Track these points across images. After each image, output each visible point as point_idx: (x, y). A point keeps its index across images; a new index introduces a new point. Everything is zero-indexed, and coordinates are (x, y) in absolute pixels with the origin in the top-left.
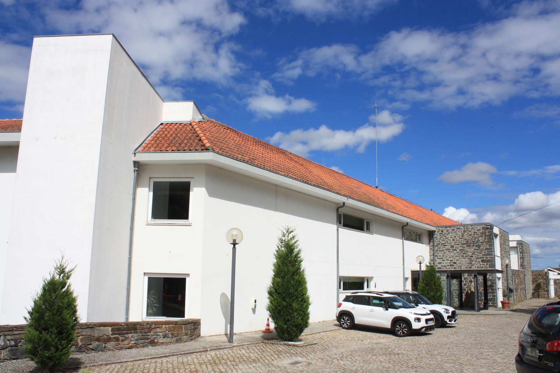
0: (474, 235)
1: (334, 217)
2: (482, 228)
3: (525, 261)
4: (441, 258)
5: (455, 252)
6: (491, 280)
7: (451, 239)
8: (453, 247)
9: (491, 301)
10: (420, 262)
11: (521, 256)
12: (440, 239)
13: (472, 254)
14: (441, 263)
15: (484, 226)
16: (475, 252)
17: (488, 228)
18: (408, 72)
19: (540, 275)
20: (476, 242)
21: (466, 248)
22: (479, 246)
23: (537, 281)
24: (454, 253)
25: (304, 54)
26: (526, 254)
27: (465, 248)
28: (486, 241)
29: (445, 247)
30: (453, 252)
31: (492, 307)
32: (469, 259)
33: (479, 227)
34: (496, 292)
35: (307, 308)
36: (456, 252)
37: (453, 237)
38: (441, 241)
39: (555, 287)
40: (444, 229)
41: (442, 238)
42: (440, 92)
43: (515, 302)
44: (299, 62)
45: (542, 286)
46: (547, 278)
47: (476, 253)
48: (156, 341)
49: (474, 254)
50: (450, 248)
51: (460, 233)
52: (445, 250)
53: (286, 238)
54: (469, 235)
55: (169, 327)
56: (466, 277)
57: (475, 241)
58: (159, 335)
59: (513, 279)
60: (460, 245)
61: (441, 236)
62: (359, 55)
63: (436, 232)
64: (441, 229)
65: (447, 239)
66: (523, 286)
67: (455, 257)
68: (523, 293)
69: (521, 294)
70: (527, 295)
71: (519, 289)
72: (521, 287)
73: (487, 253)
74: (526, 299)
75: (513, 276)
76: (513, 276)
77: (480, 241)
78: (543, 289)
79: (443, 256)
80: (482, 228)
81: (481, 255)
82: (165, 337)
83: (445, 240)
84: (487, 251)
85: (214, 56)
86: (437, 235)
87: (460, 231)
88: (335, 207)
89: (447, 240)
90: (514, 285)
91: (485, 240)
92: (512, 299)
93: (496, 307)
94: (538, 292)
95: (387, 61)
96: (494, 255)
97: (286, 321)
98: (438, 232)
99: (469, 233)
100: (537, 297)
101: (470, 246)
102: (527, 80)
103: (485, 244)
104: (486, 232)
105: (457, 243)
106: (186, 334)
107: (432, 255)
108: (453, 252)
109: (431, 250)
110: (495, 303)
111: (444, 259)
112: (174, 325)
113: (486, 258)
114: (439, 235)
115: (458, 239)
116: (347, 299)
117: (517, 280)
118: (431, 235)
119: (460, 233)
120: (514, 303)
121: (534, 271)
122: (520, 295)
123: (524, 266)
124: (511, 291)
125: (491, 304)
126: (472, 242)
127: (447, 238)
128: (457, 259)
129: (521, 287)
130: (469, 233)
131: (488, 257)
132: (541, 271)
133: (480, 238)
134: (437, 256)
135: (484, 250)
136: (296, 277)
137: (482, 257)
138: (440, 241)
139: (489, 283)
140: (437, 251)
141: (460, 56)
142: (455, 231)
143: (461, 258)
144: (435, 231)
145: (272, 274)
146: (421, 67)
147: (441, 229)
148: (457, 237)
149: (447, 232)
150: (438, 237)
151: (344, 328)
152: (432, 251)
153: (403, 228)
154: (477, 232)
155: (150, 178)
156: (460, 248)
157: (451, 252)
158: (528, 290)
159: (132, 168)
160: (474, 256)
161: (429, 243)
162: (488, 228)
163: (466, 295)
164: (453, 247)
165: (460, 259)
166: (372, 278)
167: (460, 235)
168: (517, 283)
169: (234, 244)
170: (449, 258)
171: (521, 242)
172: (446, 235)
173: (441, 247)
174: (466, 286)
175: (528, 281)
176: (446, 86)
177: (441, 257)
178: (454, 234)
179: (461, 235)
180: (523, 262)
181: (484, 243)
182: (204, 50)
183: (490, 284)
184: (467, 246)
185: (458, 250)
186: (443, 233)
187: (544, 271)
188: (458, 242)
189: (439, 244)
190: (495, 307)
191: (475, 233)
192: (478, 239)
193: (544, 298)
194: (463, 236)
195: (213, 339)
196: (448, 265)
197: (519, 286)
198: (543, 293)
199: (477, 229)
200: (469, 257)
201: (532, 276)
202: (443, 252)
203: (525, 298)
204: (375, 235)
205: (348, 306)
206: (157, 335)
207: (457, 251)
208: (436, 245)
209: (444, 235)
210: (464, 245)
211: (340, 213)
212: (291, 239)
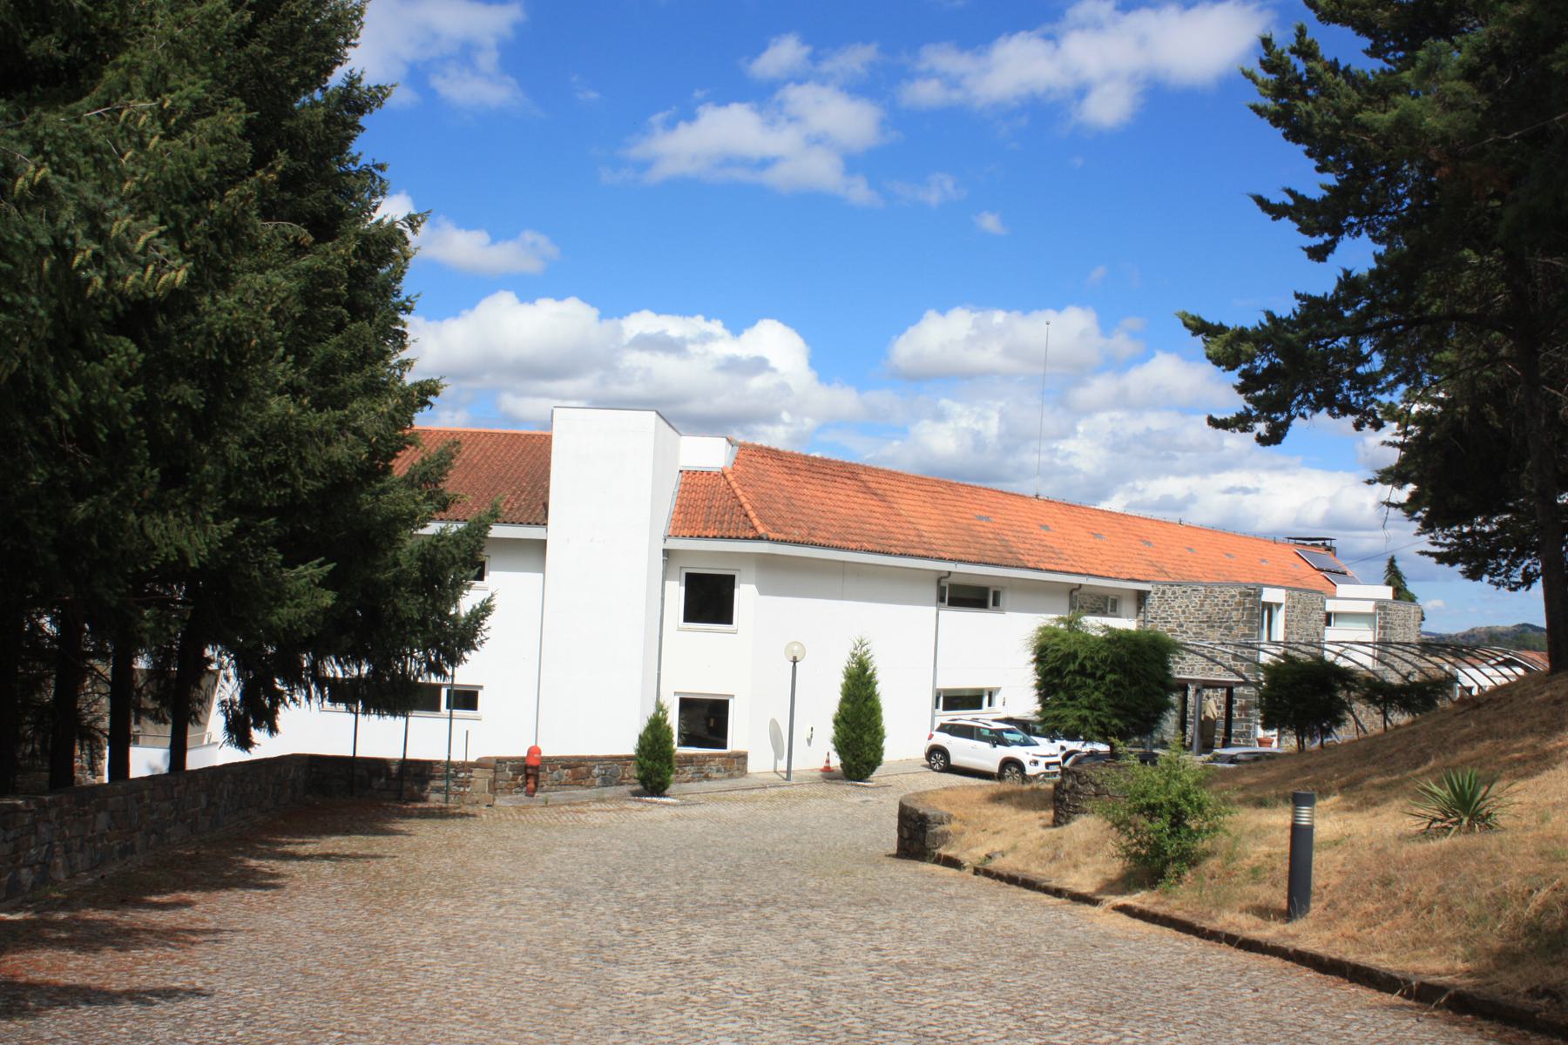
1: (933, 593)
8: (1182, 626)
15: (1243, 589)
17: (1249, 595)
22: (1230, 629)
35: (881, 741)
53: (858, 653)
64: (1162, 588)
82: (718, 771)
86: (1153, 600)
88: (935, 577)
97: (855, 757)
116: (943, 728)
133: (1234, 613)
136: (870, 704)
145: (839, 697)
147: (1162, 588)
151: (935, 770)
153: (1071, 592)
162: (1249, 595)
164: (1182, 626)
166: (999, 689)
169: (795, 661)
194: (1202, 605)
195: (760, 776)
204: (1008, 613)
205: (943, 739)
211: (942, 584)
212: (865, 654)
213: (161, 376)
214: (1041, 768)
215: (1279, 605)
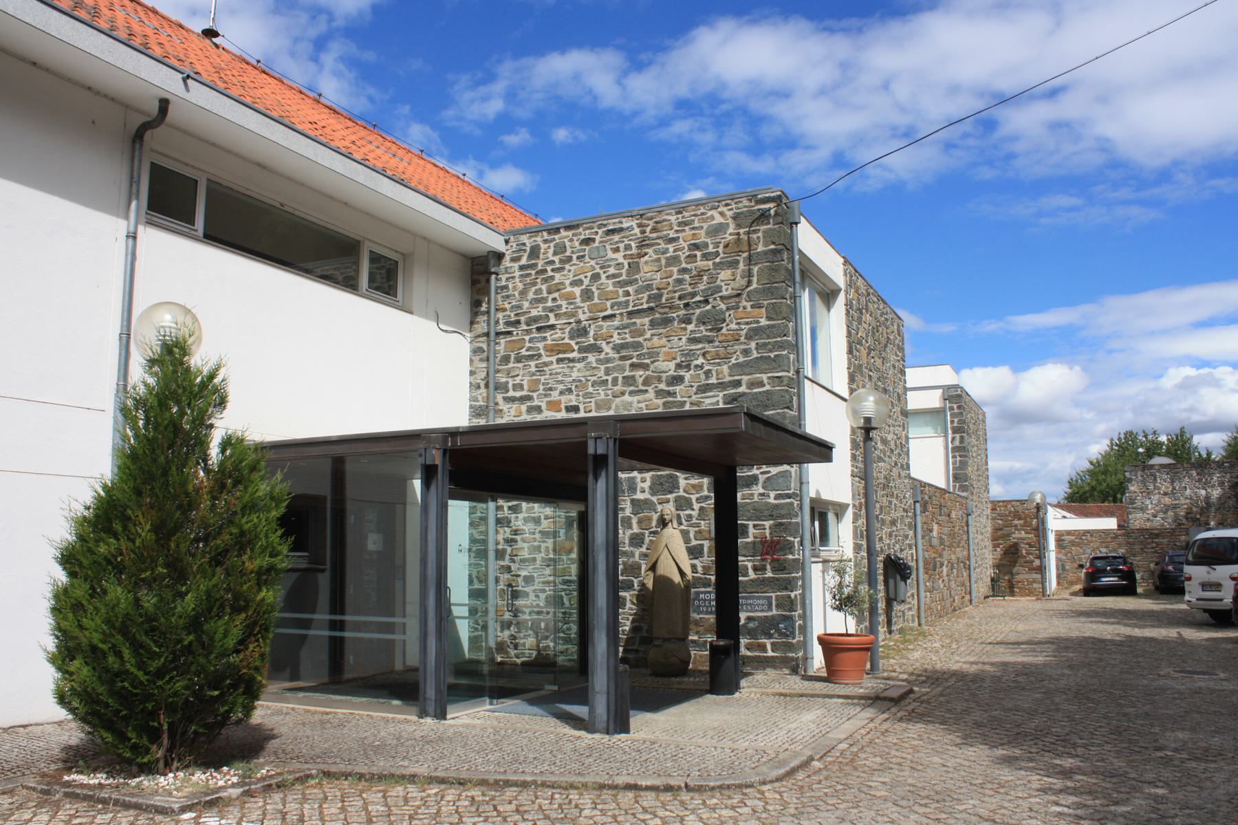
0: (691, 258)
2: (735, 218)
3: (970, 462)
5: (592, 358)
6: (760, 512)
7: (577, 291)
8: (583, 332)
9: (770, 636)
11: (957, 443)
12: (523, 293)
13: (679, 366)
16: (690, 354)
17: (763, 216)
18: (728, 114)
19: (1017, 515)
20: (698, 298)
21: (648, 335)
22: (715, 321)
23: (1009, 535)
24: (589, 367)
25: (507, 69)
26: (973, 440)
27: (642, 333)
28: (754, 286)
29: (545, 339)
30: (584, 359)
31: (775, 668)
32: (660, 393)
33: (722, 214)
34: (803, 578)
36: (599, 361)
37: (586, 282)
38: (526, 305)
39: (1060, 556)
40: (545, 241)
41: (533, 289)
42: (796, 160)
43: (923, 621)
44: (499, 87)
45: (1024, 552)
46: (1041, 527)
47: (700, 361)
49: (688, 367)
50: (567, 341)
51: (619, 257)
52: (542, 352)
54: (667, 259)
56: (646, 495)
57: (694, 295)
59: (919, 518)
60: (616, 323)
61: (528, 280)
62: (625, 73)
63: (506, 262)
65: (556, 295)
66: (961, 553)
67: (590, 389)
68: (960, 579)
69: (953, 585)
70: (974, 586)
71: (946, 563)
72: (953, 557)
73: (755, 355)
74: (971, 601)
75: (918, 505)
76: (918, 505)
77: (724, 293)
78: (1025, 562)
79: (534, 387)
80: (735, 218)
81: (725, 368)
83: (544, 300)
84: (758, 347)
85: (312, 67)
86: (509, 276)
87: (622, 246)
89: (554, 300)
90: (920, 547)
91: (749, 283)
92: (910, 609)
93: (797, 667)
94: (1012, 574)
95: (682, 91)
96: (798, 372)
98: (514, 260)
99: (665, 251)
100: (1008, 590)
101: (666, 322)
102: (971, 142)
103: (748, 305)
104: (755, 236)
105: (606, 310)
107: (482, 384)
108: (584, 359)
109: (476, 359)
110: (790, 647)
111: (536, 403)
113: (752, 385)
114: (517, 274)
115: (611, 288)
117: (935, 527)
118: (482, 278)
119: (619, 257)
120: (920, 625)
121: (999, 502)
122: (949, 588)
123: (966, 478)
124: (896, 569)
125: (770, 653)
126: (680, 298)
128: (602, 396)
129: (953, 557)
130: (665, 251)
131: (764, 377)
132: (1022, 502)
133: (725, 275)
135: (742, 339)
137: (728, 379)
138: (520, 307)
139: (753, 531)
140: (506, 359)
141: (836, 86)
142: (596, 244)
143: (623, 394)
144: (499, 256)
146: (756, 106)
148: (603, 276)
149: (555, 254)
150: (515, 288)
152: (481, 360)
154: (709, 241)
156: (616, 339)
157: (572, 360)
158: (979, 566)
160: (687, 376)
161: (472, 323)
162: (763, 216)
163: (638, 597)
165: (618, 399)
167: (619, 266)
168: (935, 542)
170: (562, 393)
171: (959, 392)
172: (550, 274)
173: (527, 338)
174: (644, 549)
175: (980, 537)
176: (809, 148)
177: (524, 393)
178: (593, 263)
179: (626, 266)
180: (963, 465)
181: (744, 303)
182: (293, 55)
183: (767, 532)
184: (653, 324)
185: (607, 349)
186: (535, 265)
187: (1033, 501)
188: (609, 304)
189: (518, 322)
190: (795, 671)
191: (696, 247)
192: (713, 279)
193: (1030, 593)
194: (634, 267)
197: (945, 553)
198: (1027, 576)
199: (705, 226)
200: (663, 386)
201: (993, 519)
202: (533, 364)
203: (967, 597)
207: (603, 356)
208: (501, 328)
209: (544, 271)
210: (638, 321)
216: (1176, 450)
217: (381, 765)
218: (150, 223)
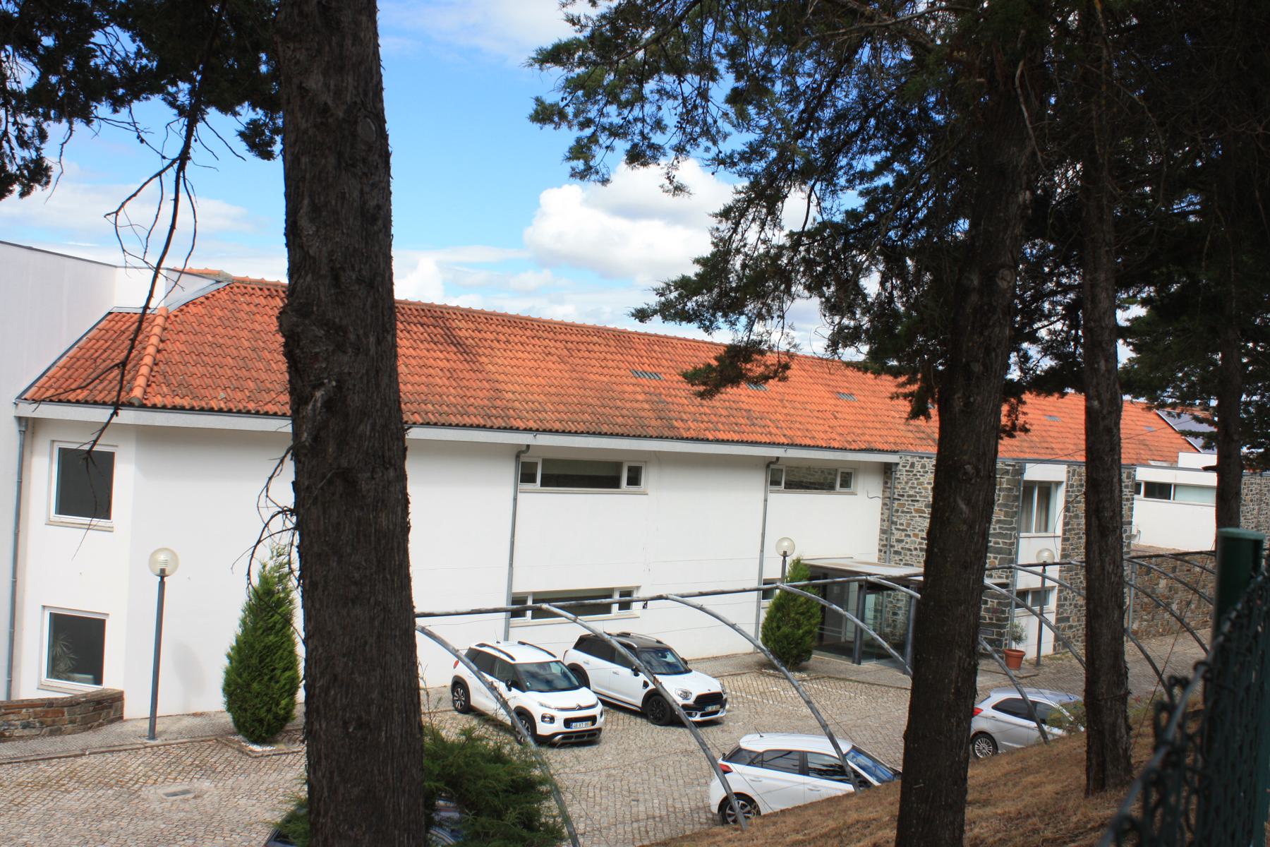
4: (903, 530)
10: (785, 553)
12: (907, 483)
14: (902, 541)
48: (7, 734)
55: (34, 712)
58: (14, 725)
63: (900, 467)
79: (909, 525)
82: (26, 726)
84: (1000, 528)
86: (902, 474)
88: (514, 453)
106: (72, 722)
112: (45, 709)
127: (921, 484)
131: (1000, 541)
134: (895, 523)
140: (897, 511)
144: (897, 464)
147: (911, 460)
153: (768, 466)
155: (53, 441)
159: (13, 429)
169: (163, 575)
196: (916, 549)
206: (10, 725)
208: (896, 496)
213: (779, 126)
214: (558, 726)
215: (1058, 484)
216: (526, 753)
217: (842, 676)
218: (772, 492)
